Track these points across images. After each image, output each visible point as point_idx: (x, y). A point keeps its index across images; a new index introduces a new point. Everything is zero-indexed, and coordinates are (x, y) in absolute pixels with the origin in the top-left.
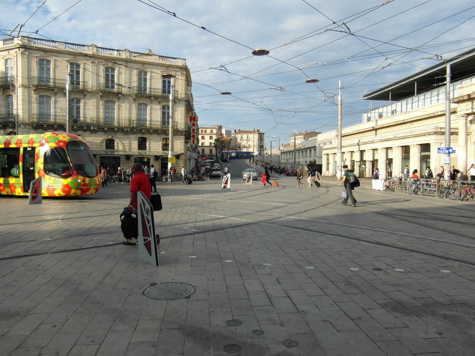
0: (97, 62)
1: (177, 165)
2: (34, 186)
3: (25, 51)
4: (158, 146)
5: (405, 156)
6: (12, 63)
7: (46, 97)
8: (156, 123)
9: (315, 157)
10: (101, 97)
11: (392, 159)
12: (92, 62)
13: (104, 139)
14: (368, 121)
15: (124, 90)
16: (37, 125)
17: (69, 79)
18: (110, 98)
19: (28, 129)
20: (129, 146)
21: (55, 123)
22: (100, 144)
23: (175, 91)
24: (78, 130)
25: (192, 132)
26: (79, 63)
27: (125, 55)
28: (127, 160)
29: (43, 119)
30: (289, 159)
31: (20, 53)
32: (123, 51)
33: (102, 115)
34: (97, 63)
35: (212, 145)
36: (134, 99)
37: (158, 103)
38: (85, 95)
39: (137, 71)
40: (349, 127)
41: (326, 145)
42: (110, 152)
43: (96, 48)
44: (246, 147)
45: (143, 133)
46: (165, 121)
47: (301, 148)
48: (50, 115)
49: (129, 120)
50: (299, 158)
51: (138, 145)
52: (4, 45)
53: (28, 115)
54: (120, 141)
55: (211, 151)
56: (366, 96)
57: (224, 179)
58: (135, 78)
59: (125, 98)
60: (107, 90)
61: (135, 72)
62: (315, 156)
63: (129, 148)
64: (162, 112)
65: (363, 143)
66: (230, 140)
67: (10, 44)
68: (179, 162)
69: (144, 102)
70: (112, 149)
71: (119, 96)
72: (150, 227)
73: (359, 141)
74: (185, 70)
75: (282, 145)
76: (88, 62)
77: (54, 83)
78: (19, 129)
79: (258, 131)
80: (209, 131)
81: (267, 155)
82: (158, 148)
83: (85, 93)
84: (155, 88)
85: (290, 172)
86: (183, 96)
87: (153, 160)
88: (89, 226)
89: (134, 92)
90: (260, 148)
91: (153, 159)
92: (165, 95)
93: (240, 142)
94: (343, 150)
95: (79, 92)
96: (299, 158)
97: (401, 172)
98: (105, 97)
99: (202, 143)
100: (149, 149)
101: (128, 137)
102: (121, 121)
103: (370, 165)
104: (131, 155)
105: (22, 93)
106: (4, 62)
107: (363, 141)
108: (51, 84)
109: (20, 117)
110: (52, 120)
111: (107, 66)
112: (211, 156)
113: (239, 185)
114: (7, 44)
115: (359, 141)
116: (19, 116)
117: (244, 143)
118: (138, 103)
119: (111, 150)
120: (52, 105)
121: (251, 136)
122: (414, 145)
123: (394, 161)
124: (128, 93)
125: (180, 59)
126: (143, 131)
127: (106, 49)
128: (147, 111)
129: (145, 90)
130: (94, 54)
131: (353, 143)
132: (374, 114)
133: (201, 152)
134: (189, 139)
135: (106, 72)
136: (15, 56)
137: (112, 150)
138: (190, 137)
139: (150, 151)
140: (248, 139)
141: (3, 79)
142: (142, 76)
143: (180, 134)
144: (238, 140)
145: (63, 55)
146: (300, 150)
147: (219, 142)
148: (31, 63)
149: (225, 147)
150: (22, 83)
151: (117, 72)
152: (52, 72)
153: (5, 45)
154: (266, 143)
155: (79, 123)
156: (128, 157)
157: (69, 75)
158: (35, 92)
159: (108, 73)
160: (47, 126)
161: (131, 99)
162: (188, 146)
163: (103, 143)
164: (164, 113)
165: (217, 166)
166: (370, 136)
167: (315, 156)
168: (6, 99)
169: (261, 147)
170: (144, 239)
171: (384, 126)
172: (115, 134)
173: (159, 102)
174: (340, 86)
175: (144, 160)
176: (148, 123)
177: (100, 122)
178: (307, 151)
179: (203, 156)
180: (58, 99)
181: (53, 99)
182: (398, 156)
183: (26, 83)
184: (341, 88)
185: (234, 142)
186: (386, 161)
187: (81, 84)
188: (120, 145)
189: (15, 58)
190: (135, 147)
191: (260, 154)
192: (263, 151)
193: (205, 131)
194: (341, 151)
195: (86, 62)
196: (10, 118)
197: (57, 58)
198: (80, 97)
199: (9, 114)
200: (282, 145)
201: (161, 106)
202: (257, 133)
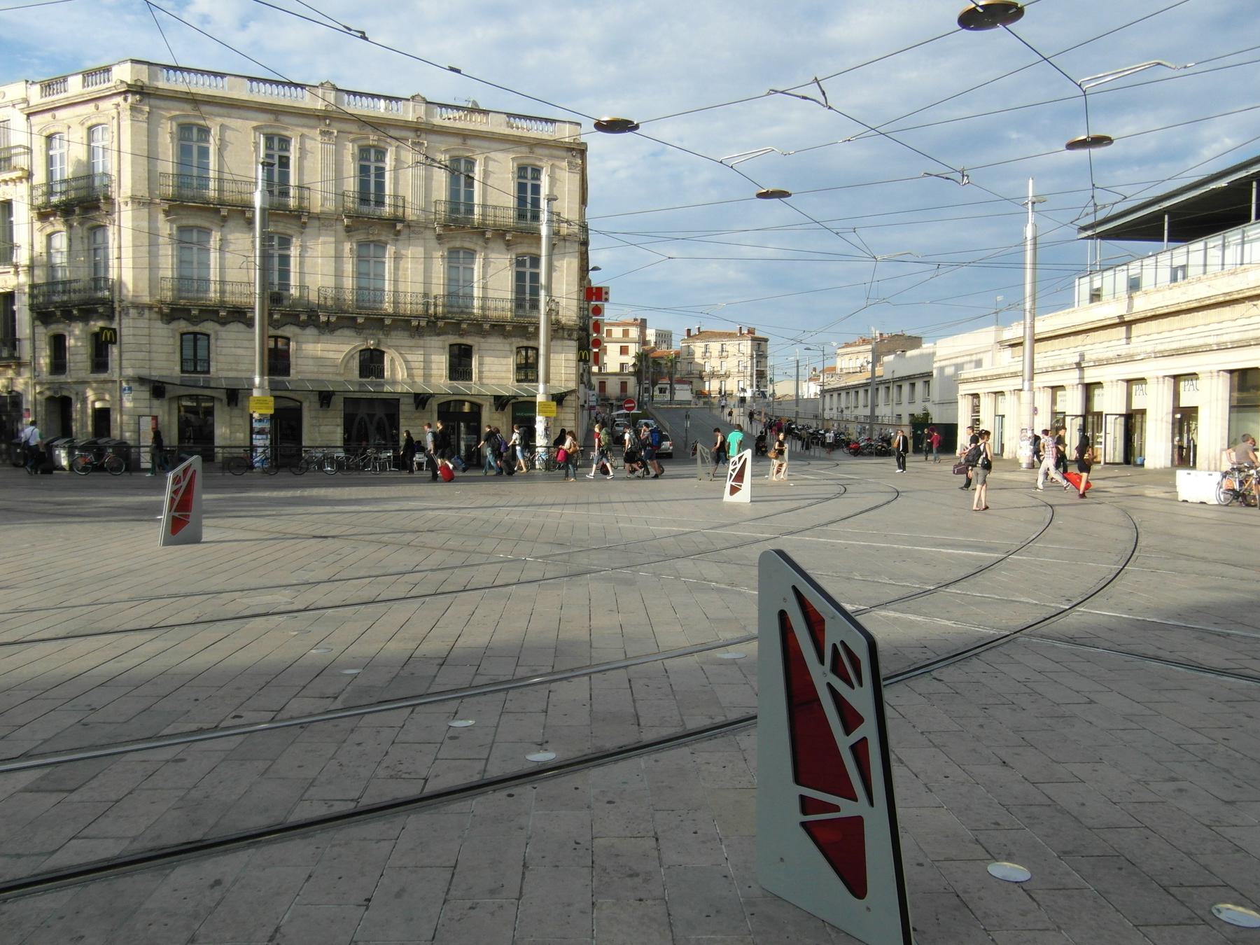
0: (335, 132)
2: (179, 485)
3: (140, 101)
4: (504, 368)
5: (1239, 400)
6: (106, 137)
7: (199, 231)
8: (500, 304)
10: (348, 229)
11: (1194, 410)
12: (324, 132)
13: (355, 348)
14: (1092, 300)
15: (411, 214)
16: (173, 310)
17: (263, 176)
19: (150, 320)
20: (424, 369)
21: (222, 304)
22: (345, 361)
26: (287, 133)
27: (414, 111)
28: (417, 408)
29: (189, 291)
30: (847, 408)
31: (128, 107)
32: (408, 100)
33: (349, 283)
34: (336, 134)
35: (626, 371)
36: (439, 237)
37: (503, 247)
38: (304, 225)
42: (371, 384)
43: (333, 93)
44: (719, 377)
45: (463, 334)
46: (524, 299)
47: (884, 378)
48: (209, 280)
49: (426, 295)
51: (448, 365)
52: (84, 87)
53: (147, 282)
54: (400, 354)
55: (624, 385)
56: (1085, 229)
57: (731, 467)
59: (414, 232)
60: (365, 209)
61: (350, 149)
63: (424, 375)
64: (514, 274)
65: (1094, 362)
67: (100, 83)
69: (467, 245)
70: (377, 377)
71: (396, 226)
72: (859, 749)
73: (1082, 356)
74: (579, 155)
76: (313, 131)
77: (221, 190)
78: (123, 321)
80: (617, 332)
82: (503, 374)
84: (495, 204)
85: (863, 444)
87: (490, 409)
88: (398, 648)
93: (702, 362)
95: (287, 215)
97: (1226, 447)
98: (358, 229)
100: (480, 378)
101: (421, 342)
102: (402, 300)
103: (1118, 426)
104: (432, 395)
105: (133, 220)
106: (84, 133)
107: (1094, 357)
108: (212, 193)
109: (127, 289)
110: (212, 295)
111: (365, 143)
112: (624, 399)
114: (92, 85)
115: (1082, 356)
116: (125, 285)
117: (711, 365)
118: (448, 249)
119: (374, 379)
120: (214, 257)
121: (731, 346)
122: (1211, 372)
123: (1201, 414)
125: (564, 122)
126: (464, 326)
127: (361, 94)
129: (470, 210)
131: (1060, 362)
132: (1112, 282)
135: (362, 159)
136: (113, 118)
137: (378, 380)
139: (482, 385)
140: (724, 354)
141: (82, 183)
142: (460, 173)
143: (566, 336)
144: (696, 356)
145: (242, 112)
148: (157, 134)
150: (132, 190)
151: (391, 161)
152: (215, 161)
153: (88, 86)
155: (285, 302)
156: (421, 400)
157: (263, 164)
158: (167, 216)
160: (201, 311)
161: (429, 235)
163: (351, 361)
164: (520, 277)
166: (1114, 342)
168: (89, 238)
170: (803, 798)
171: (1158, 313)
172: (387, 335)
173: (509, 245)
174: (1031, 194)
176: (476, 303)
177: (345, 300)
178: (900, 387)
180: (230, 237)
181: (215, 238)
182: (1217, 400)
183: (143, 192)
184: (1034, 199)
186: (1174, 413)
187: (292, 192)
188: (400, 365)
189: (115, 121)
192: (766, 386)
195: (305, 131)
196: (101, 289)
197: (227, 121)
198: (289, 232)
199: (98, 279)
201: (514, 257)
202: (749, 336)
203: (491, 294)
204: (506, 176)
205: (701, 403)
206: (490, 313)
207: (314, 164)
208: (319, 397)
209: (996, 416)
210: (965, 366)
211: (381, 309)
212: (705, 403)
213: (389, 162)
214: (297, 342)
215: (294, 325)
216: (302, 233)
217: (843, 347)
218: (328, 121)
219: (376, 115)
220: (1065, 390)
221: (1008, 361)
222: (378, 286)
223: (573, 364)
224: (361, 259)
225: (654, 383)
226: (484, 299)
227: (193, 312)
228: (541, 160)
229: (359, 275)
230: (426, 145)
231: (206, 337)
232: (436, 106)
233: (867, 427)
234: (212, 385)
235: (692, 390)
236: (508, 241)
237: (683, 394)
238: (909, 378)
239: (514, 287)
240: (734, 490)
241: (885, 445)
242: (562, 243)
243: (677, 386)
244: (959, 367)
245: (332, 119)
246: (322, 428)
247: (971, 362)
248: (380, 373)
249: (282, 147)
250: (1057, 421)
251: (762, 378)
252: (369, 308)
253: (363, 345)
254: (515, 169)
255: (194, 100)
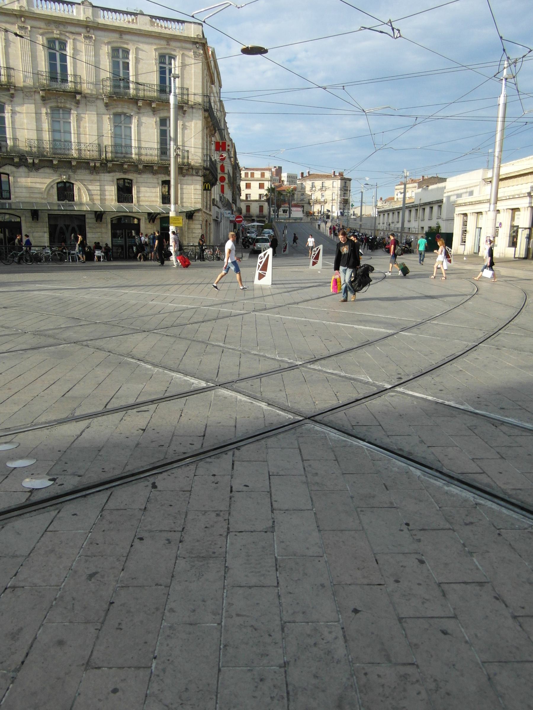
1: (190, 231)
4: (154, 195)
8: (150, 152)
9: (440, 221)
10: (44, 99)
13: (53, 181)
15: (86, 88)
18: (61, 103)
20: (100, 195)
22: (47, 190)
23: (184, 88)
24: (5, 165)
25: (219, 170)
27: (84, 13)
30: (393, 223)
32: (79, 4)
33: (46, 136)
34: (29, 29)
36: (107, 105)
37: (151, 113)
38: (12, 96)
39: (110, 47)
40: (511, 163)
41: (461, 197)
44: (320, 203)
45: (125, 172)
47: (415, 204)
49: (99, 145)
50: (409, 221)
54: (84, 185)
55: (261, 208)
57: (259, 261)
58: (106, 63)
59: (89, 101)
61: (105, 50)
62: (439, 218)
64: (159, 131)
66: (292, 191)
68: (192, 226)
69: (125, 111)
74: (201, 47)
75: (381, 199)
76: (13, 26)
79: (341, 174)
80: (257, 175)
81: (355, 217)
82: (154, 199)
83: (12, 91)
86: (199, 99)
89: (104, 91)
90: (344, 204)
91: (145, 219)
92: (163, 96)
93: (310, 193)
94: (500, 206)
96: (409, 221)
99: (247, 195)
100: (138, 201)
101: (98, 177)
111: (51, 36)
113: (297, 270)
117: (316, 195)
119: (68, 202)
121: (328, 183)
124: (94, 93)
126: (126, 166)
128: (130, 128)
130: (23, 9)
131: (518, 192)
133: (244, 211)
134: (213, 184)
137: (70, 202)
138: (216, 180)
140: (314, 189)
143: (194, 173)
144: (306, 190)
146: (413, 207)
147: (274, 193)
149: (284, 202)
151: (70, 50)
154: (354, 198)
156: (99, 216)
159: (54, 51)
161: (101, 105)
162: (213, 197)
163: (51, 190)
165: (268, 233)
167: (439, 218)
169: (345, 203)
173: (154, 111)
175: (134, 222)
177: (44, 148)
178: (424, 209)
179: (249, 218)
185: (300, 193)
188: (84, 192)
190: (111, 197)
191: (342, 214)
192: (349, 209)
193: (252, 175)
194: (495, 207)
200: (381, 199)
201: (158, 119)
202: (340, 178)
203: (143, 145)
204: (151, 62)
205: (309, 219)
206: (143, 158)
207: (16, 51)
208: (95, 215)
209: (477, 228)
210: (463, 195)
211: (69, 155)
212: (311, 219)
213: (69, 51)
214: (14, 177)
215: (11, 165)
216: (11, 101)
217: (399, 185)
218: (23, 19)
219: (57, 15)
220: (519, 211)
221: (487, 191)
222: (67, 139)
223: (200, 192)
224: (54, 121)
225: (279, 207)
226: (139, 148)
227: (91, 164)
228: (174, 50)
229: (53, 131)
230: (94, 38)
231: (7, 176)
232: (99, 9)
233: (399, 235)
234: (13, 207)
235: (303, 211)
236: (154, 108)
237: (297, 213)
238: (429, 203)
239: (159, 140)
240: (261, 276)
241: (407, 246)
242: (190, 110)
243: (293, 209)
244: (459, 196)
245: (26, 17)
246: (35, 233)
247: (466, 192)
248: (71, 198)
249: (61, 47)
250: (514, 232)
251: (347, 204)
252: (61, 154)
253: (59, 179)
254: (157, 57)
255: (121, 32)
